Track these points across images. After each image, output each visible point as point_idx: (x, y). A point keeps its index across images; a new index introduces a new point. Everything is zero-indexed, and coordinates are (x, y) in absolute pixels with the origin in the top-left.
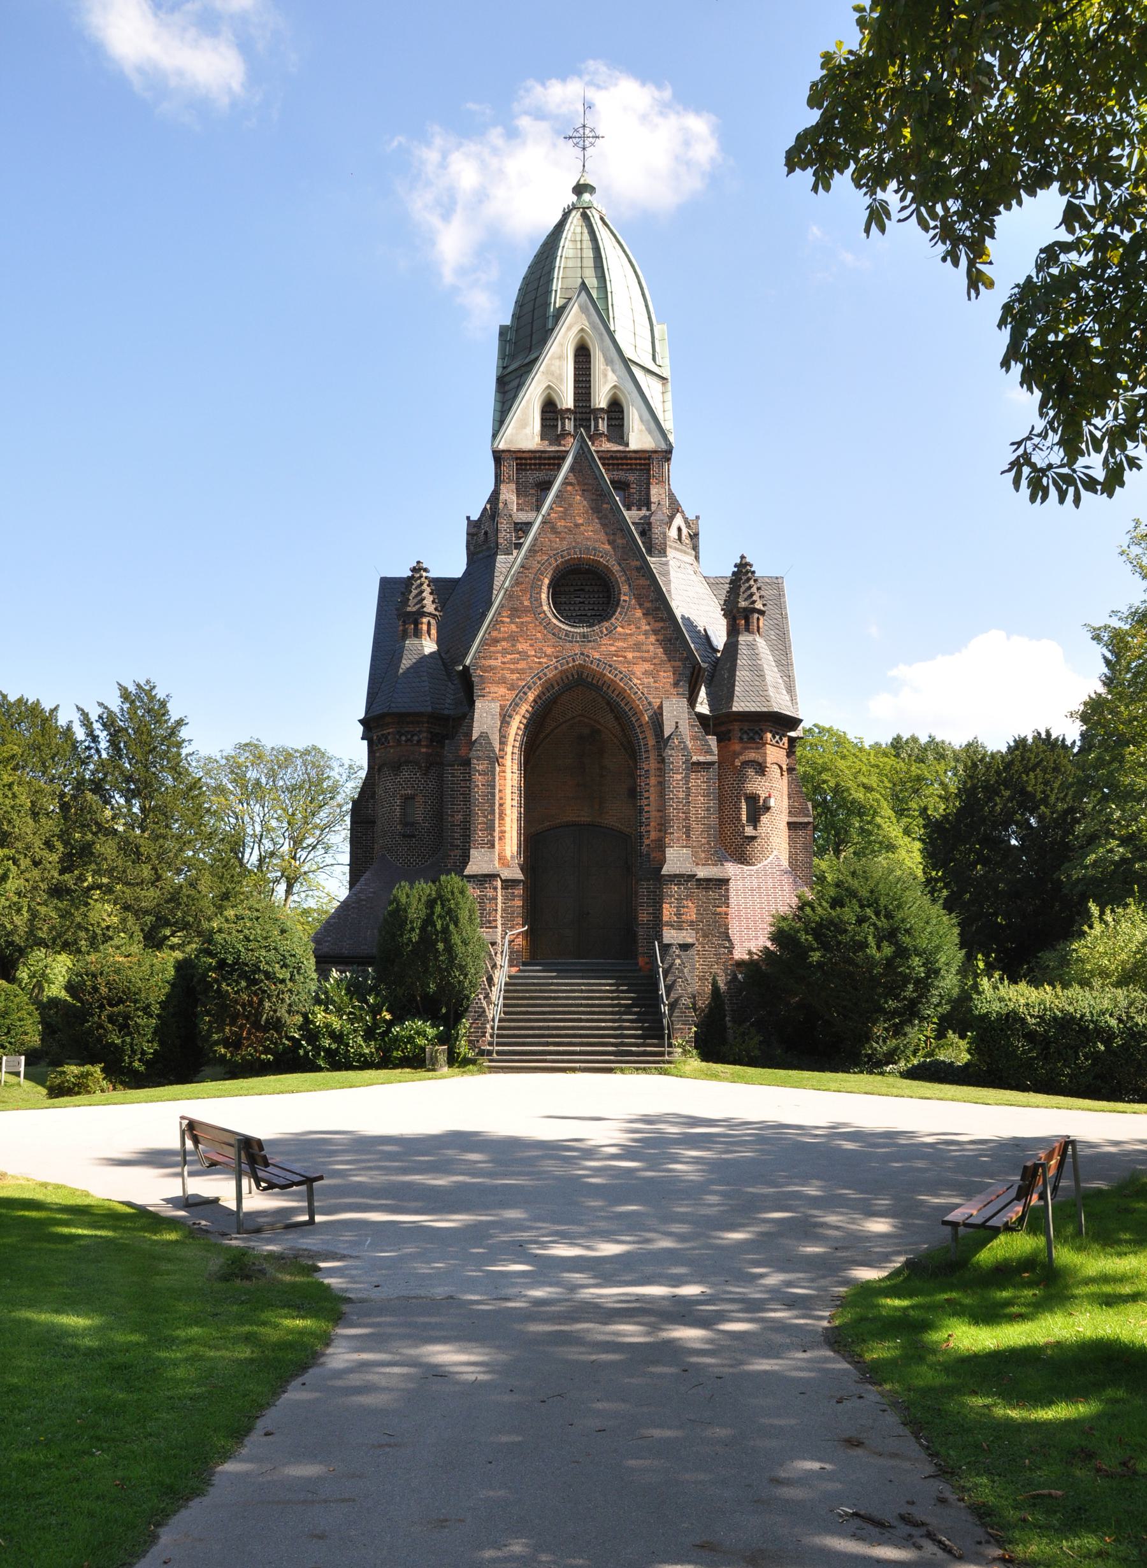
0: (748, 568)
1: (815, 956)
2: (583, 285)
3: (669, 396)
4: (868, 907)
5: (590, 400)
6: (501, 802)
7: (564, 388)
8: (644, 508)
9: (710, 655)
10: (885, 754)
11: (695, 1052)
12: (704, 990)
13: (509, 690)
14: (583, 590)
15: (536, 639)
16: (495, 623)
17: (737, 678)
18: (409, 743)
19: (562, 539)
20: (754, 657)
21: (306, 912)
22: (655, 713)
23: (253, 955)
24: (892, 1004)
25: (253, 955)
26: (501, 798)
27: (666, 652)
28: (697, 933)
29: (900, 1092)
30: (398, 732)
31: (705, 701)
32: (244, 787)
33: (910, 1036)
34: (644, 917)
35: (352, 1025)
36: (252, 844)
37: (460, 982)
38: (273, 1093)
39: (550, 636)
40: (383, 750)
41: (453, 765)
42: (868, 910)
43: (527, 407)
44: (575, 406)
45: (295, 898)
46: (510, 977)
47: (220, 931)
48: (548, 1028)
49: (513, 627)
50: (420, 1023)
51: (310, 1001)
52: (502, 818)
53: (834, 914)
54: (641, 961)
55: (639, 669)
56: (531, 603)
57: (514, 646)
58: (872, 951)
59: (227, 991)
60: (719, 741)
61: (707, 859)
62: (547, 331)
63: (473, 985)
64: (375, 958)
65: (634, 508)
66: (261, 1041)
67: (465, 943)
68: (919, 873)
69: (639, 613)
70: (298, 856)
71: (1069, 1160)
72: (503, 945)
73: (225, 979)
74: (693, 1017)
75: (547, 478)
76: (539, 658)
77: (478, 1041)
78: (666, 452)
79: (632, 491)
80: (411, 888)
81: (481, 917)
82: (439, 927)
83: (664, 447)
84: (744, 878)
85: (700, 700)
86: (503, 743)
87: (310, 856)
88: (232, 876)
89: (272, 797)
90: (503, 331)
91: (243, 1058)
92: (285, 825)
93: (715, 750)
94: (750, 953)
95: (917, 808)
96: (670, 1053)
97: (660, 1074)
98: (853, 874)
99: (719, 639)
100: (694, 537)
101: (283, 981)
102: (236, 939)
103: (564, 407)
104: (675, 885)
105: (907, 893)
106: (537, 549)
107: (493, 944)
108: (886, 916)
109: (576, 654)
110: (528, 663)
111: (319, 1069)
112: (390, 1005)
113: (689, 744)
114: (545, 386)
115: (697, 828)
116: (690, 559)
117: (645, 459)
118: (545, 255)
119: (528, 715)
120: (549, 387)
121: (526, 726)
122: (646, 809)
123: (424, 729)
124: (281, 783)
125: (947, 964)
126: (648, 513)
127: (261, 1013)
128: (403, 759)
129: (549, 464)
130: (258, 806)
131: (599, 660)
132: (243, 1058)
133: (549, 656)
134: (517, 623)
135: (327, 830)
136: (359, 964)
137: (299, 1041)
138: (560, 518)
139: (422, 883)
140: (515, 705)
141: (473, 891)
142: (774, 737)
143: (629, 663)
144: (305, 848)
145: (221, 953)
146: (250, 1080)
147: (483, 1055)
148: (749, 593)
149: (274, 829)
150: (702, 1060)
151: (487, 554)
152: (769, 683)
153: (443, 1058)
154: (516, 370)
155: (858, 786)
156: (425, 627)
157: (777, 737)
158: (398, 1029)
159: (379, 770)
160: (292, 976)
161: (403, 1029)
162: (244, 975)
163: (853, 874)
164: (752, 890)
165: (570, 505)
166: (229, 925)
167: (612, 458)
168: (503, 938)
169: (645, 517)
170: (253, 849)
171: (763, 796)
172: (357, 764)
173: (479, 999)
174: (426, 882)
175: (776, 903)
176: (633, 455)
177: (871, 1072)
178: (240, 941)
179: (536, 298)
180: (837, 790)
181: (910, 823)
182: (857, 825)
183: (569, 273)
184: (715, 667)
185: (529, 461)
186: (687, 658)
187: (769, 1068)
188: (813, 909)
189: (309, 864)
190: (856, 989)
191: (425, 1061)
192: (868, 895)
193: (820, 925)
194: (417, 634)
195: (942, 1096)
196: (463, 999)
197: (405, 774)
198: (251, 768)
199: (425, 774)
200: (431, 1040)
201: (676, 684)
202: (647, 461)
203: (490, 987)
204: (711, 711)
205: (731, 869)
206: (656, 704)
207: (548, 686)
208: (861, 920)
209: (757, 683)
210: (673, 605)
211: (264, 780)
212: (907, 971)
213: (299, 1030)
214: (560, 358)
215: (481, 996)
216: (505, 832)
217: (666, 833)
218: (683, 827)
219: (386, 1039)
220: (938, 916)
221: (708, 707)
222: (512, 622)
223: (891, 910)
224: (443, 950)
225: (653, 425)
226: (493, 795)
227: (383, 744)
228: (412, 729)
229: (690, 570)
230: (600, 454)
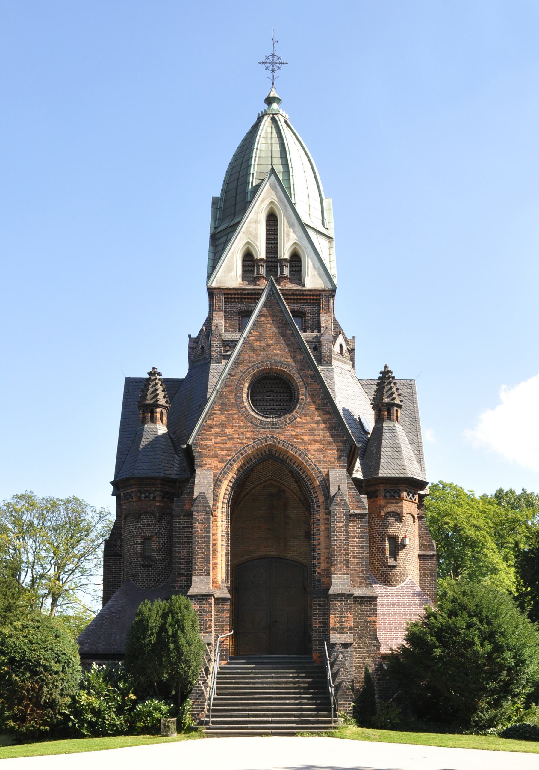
0: (390, 374)
1: (438, 652)
2: (273, 171)
3: (333, 251)
4: (475, 616)
5: (277, 253)
6: (214, 542)
7: (258, 244)
8: (316, 331)
9: (363, 436)
10: (490, 503)
11: (353, 720)
12: (359, 676)
13: (219, 462)
14: (272, 391)
15: (239, 426)
16: (211, 414)
17: (382, 453)
18: (147, 499)
19: (258, 355)
20: (394, 438)
21: (67, 619)
22: (324, 479)
23: (35, 654)
24: (492, 685)
25: (35, 654)
26: (214, 540)
27: (332, 435)
28: (354, 635)
29: (497, 747)
30: (139, 491)
31: (360, 469)
32: (21, 527)
33: (505, 707)
34: (316, 624)
35: (107, 703)
36: (26, 569)
37: (185, 672)
38: (52, 754)
39: (249, 424)
40: (128, 504)
41: (180, 516)
42: (475, 619)
43: (232, 257)
44: (266, 257)
45: (59, 609)
46: (221, 668)
47: (10, 636)
48: (249, 705)
49: (223, 417)
50: (156, 702)
51: (77, 687)
52: (215, 554)
53: (450, 621)
54: (315, 656)
55: (313, 448)
56: (236, 400)
57: (223, 431)
58: (478, 647)
59: (16, 680)
60: (369, 498)
61: (361, 583)
62: (246, 203)
63: (195, 674)
64: (124, 655)
65: (309, 331)
66: (40, 717)
67: (189, 644)
68: (514, 589)
69: (312, 408)
70: (61, 577)
72: (216, 645)
73: (14, 671)
74: (351, 695)
75: (246, 309)
76: (241, 440)
77: (198, 715)
78: (331, 290)
79: (307, 318)
80: (152, 604)
81: (200, 625)
82: (170, 633)
83: (330, 287)
84: (387, 596)
85: (355, 468)
86: (215, 500)
87: (70, 578)
88: (13, 594)
89: (42, 534)
90: (215, 201)
91: (27, 729)
92: (52, 555)
93: (366, 505)
94: (392, 650)
95: (513, 541)
96: (335, 722)
97: (329, 736)
98: (464, 593)
99: (370, 425)
100: (352, 351)
101: (57, 673)
102: (22, 642)
103: (259, 257)
104: (339, 601)
105: (502, 607)
106: (240, 362)
107: (209, 644)
108: (487, 623)
109: (267, 437)
110: (233, 443)
111: (83, 736)
112: (135, 689)
113: (348, 501)
114: (245, 242)
115: (354, 561)
116: (349, 367)
117: (316, 296)
118: (245, 148)
119: (233, 481)
120: (248, 243)
121: (232, 488)
124: (49, 524)
125: (530, 657)
126: (319, 334)
127: (40, 696)
129: (248, 299)
130: (31, 540)
131: (284, 441)
132: (27, 729)
133: (249, 438)
134: (225, 414)
135: (83, 558)
136: (113, 659)
137: (68, 716)
138: (256, 340)
139: (160, 601)
140: (224, 473)
141: (194, 607)
142: (409, 495)
143: (305, 443)
144: (67, 572)
145: (11, 652)
146: (33, 745)
147: (202, 725)
148: (390, 392)
149: (43, 558)
150: (359, 726)
151: (203, 362)
152: (404, 456)
153: (173, 727)
154: (224, 230)
155: (471, 526)
156: (158, 415)
157: (411, 495)
158: (140, 707)
159: (125, 518)
160: (63, 669)
161: (144, 706)
162: (28, 669)
163: (464, 593)
164: (393, 604)
165: (264, 331)
166: (17, 632)
167: (293, 294)
168: (216, 640)
169: (316, 337)
170: (27, 572)
171: (401, 537)
172: (106, 511)
173: (199, 684)
174: (162, 601)
175: (410, 613)
176: (309, 293)
177: (478, 734)
178: (26, 644)
179: (238, 179)
180: (456, 529)
181: (508, 553)
182: (470, 554)
183: (263, 161)
184: (367, 444)
185: (233, 296)
186: (346, 440)
187: (406, 731)
188: (436, 618)
189: (69, 583)
190: (467, 675)
191: (160, 729)
192: (475, 608)
193: (441, 629)
194: (153, 420)
195: (526, 749)
196: (188, 685)
197: (144, 521)
198: (26, 513)
199: (158, 521)
200: (165, 714)
201: (339, 459)
202: (318, 297)
203: (207, 675)
204: (363, 476)
205: (378, 589)
206: (324, 474)
207: (248, 460)
208: (469, 626)
209: (396, 457)
210: (337, 402)
211: (36, 522)
212: (502, 661)
213: (69, 708)
214: (256, 222)
215: (201, 682)
216: (217, 564)
217: (331, 565)
218: (344, 560)
219: (132, 714)
220: (524, 623)
221: (361, 474)
222: (222, 414)
223: (491, 619)
224: (173, 649)
225: (322, 271)
226: (209, 537)
227: (128, 499)
228: (148, 489)
229: (349, 375)
230: (284, 292)
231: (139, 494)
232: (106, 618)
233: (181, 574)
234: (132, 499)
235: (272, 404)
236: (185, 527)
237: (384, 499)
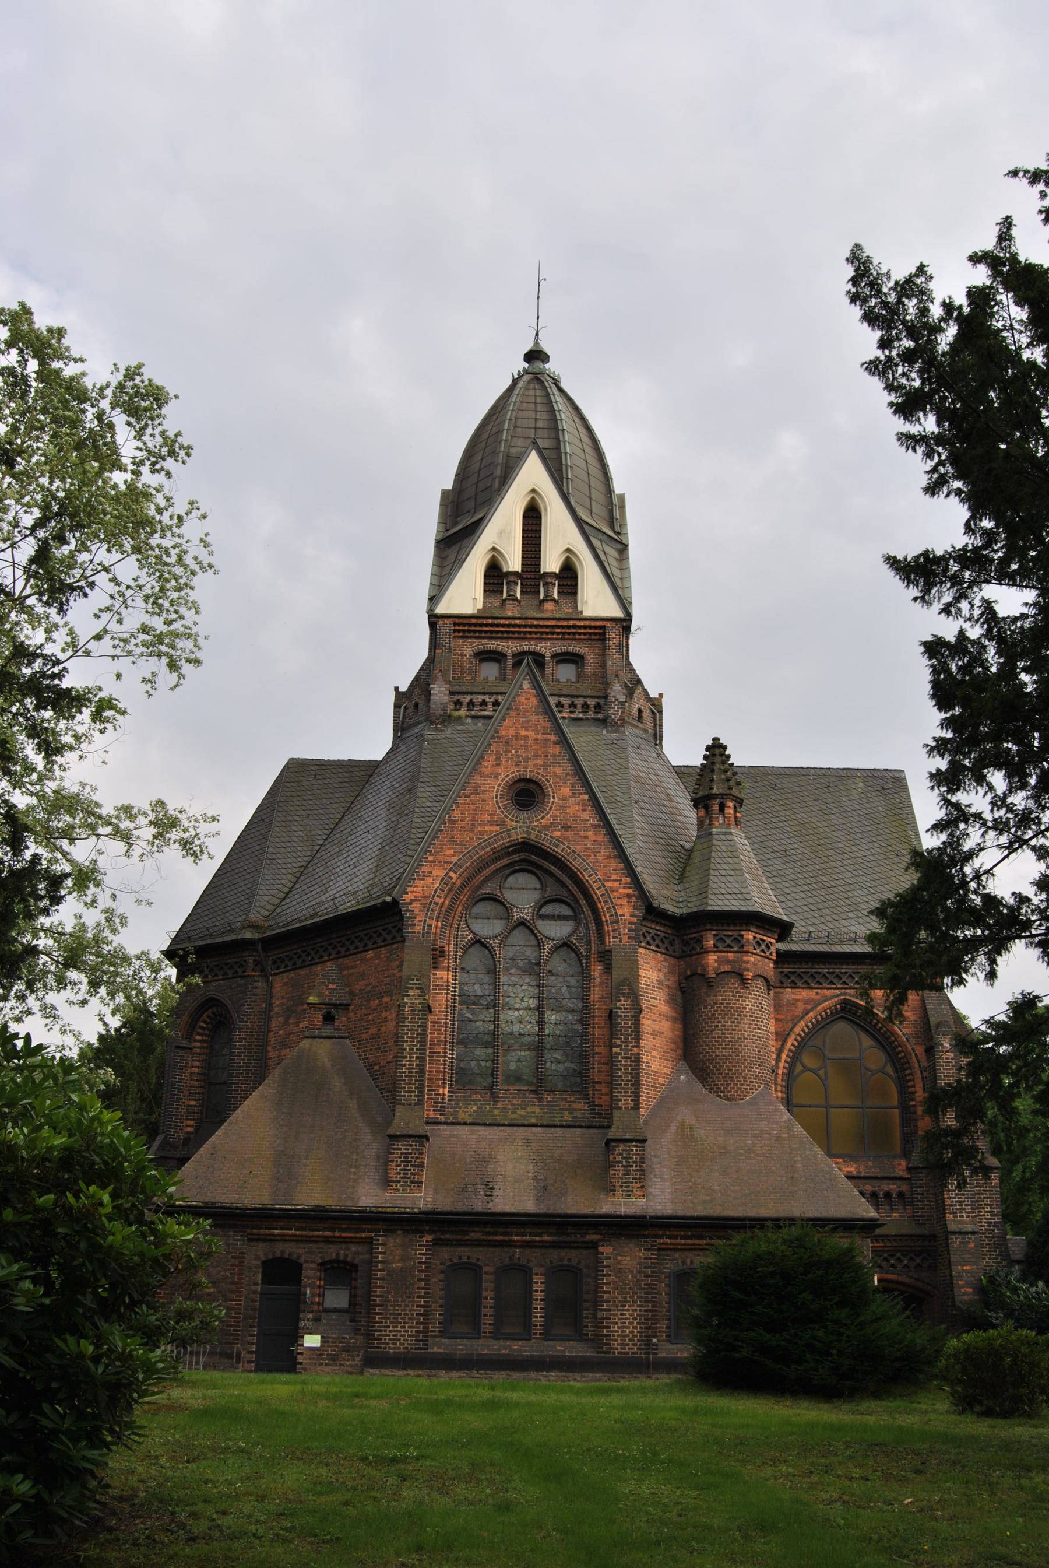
90: (445, 494)
179: (480, 470)
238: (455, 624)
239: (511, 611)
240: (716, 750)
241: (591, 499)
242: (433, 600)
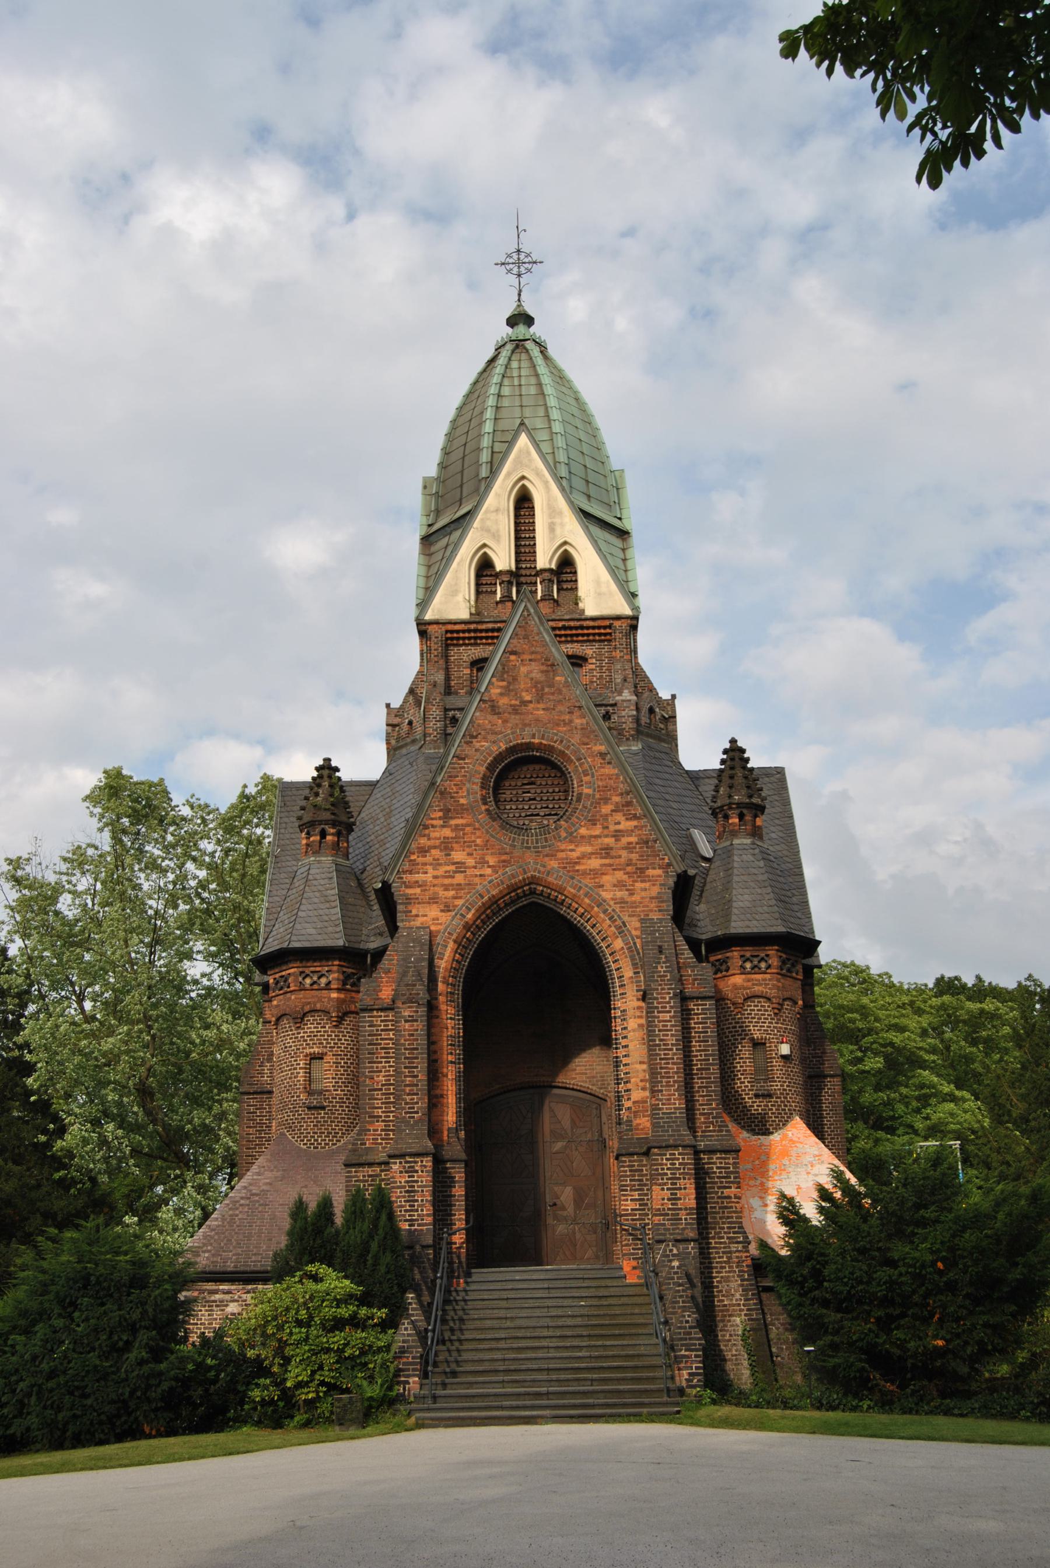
13: (442, 911)
15: (476, 845)
30: (302, 973)
71: (443, 1253)
110: (465, 876)
117: (605, 627)
122: (625, 1061)
123: (335, 968)
128: (307, 1008)
129: (487, 638)
165: (515, 679)
179: (463, 458)
185: (461, 635)
197: (311, 1026)
199: (335, 1026)
231: (300, 979)
232: (241, 1205)
233: (374, 1117)
234: (289, 987)
235: (533, 807)
236: (382, 1030)
237: (741, 974)
238: (447, 632)
239: (445, 1057)
240: (735, 754)
241: (587, 482)
242: (423, 604)
